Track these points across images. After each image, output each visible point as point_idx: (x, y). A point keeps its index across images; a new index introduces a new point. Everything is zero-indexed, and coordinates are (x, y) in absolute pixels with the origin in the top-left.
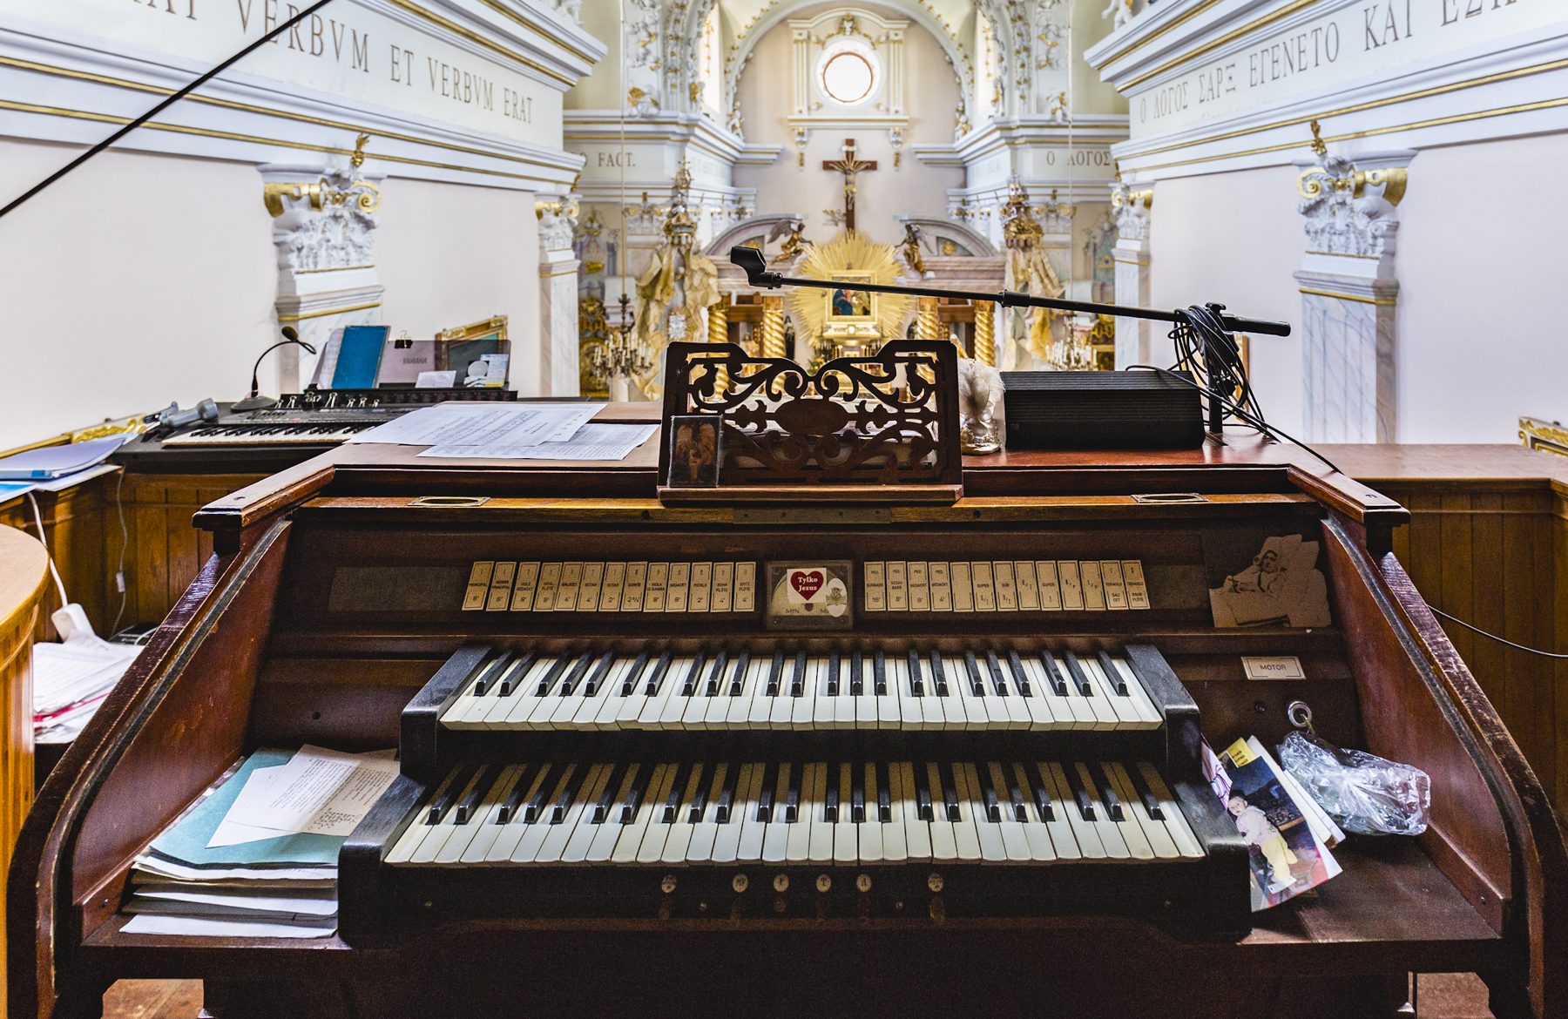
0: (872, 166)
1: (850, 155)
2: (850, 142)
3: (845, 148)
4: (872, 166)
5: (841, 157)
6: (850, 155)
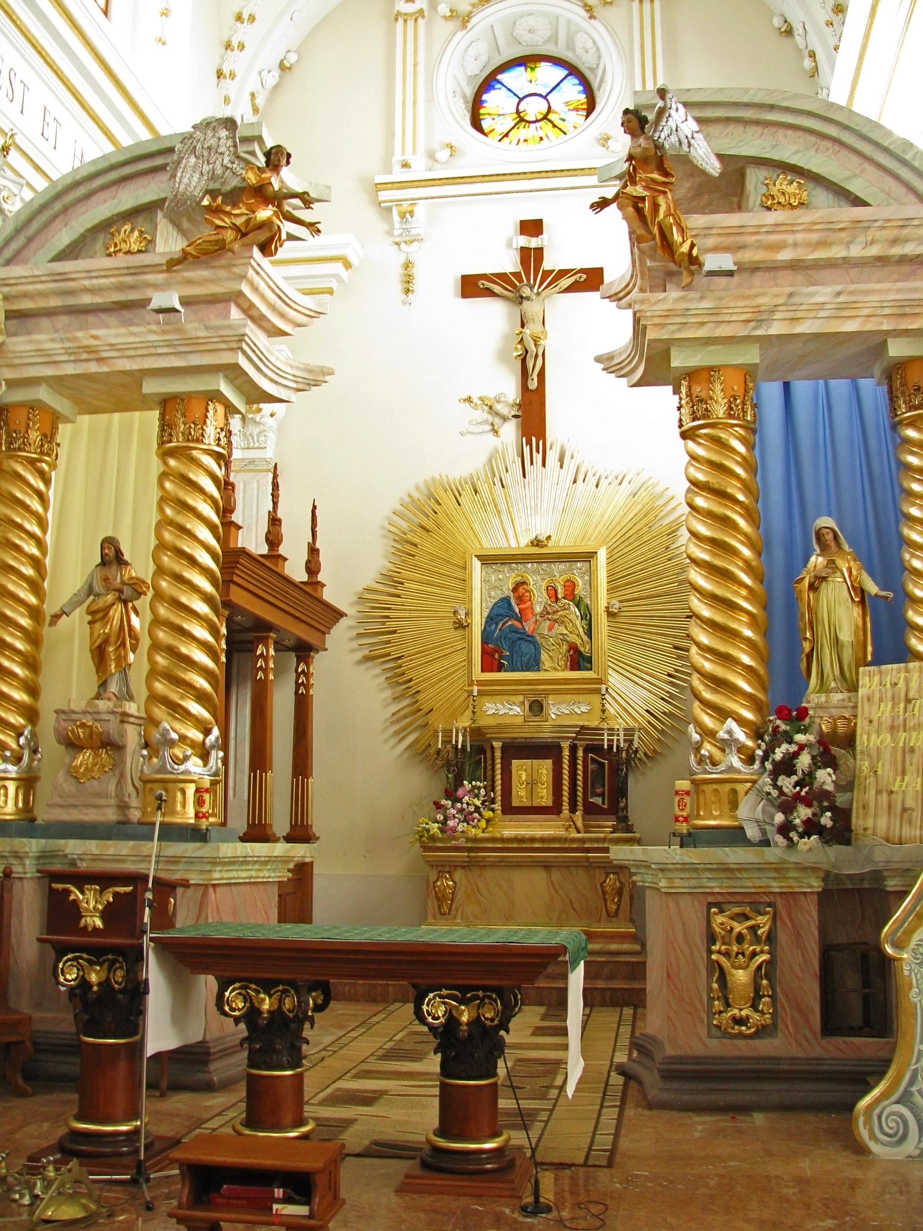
0: (472, 286)
1: (531, 258)
2: (532, 227)
3: (524, 241)
4: (472, 286)
5: (509, 264)
6: (531, 258)
